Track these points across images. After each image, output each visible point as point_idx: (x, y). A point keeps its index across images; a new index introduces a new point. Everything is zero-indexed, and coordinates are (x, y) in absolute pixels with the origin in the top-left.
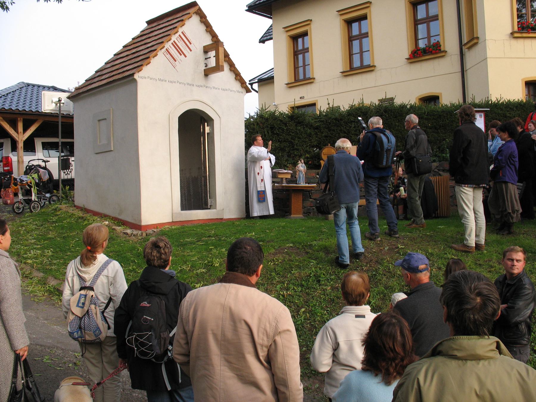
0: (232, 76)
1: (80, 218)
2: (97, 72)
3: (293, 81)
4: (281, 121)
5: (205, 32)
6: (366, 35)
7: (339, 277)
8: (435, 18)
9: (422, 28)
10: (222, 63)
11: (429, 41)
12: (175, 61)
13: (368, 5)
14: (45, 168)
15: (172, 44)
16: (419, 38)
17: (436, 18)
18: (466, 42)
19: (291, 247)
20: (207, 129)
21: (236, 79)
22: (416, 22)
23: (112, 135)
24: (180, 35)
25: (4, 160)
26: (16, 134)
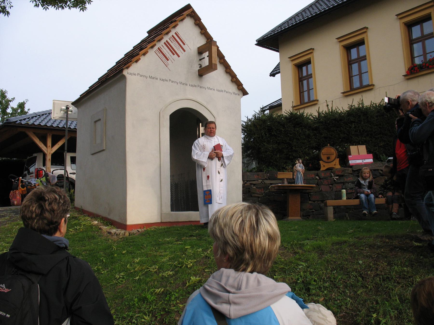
3: (299, 104)
4: (279, 123)
5: (200, 34)
6: (364, 58)
7: (335, 285)
11: (425, 58)
12: (168, 60)
15: (165, 43)
16: (415, 56)
21: (232, 81)
22: (411, 42)
24: (173, 36)
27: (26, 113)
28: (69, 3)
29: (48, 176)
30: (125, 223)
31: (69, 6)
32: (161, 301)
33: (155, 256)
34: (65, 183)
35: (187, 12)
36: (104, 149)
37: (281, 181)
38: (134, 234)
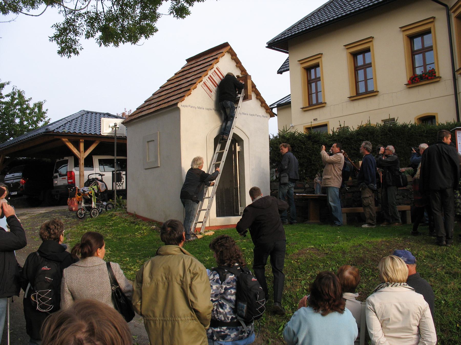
1: (132, 223)
2: (146, 102)
3: (307, 105)
4: (300, 141)
6: (370, 65)
8: (430, 49)
9: (418, 58)
10: (250, 93)
11: (425, 68)
12: (211, 92)
14: (101, 181)
15: (209, 78)
16: (416, 66)
17: (430, 49)
18: (458, 69)
19: (312, 248)
20: (238, 149)
22: (413, 53)
23: (159, 154)
24: (215, 71)
25: (68, 174)
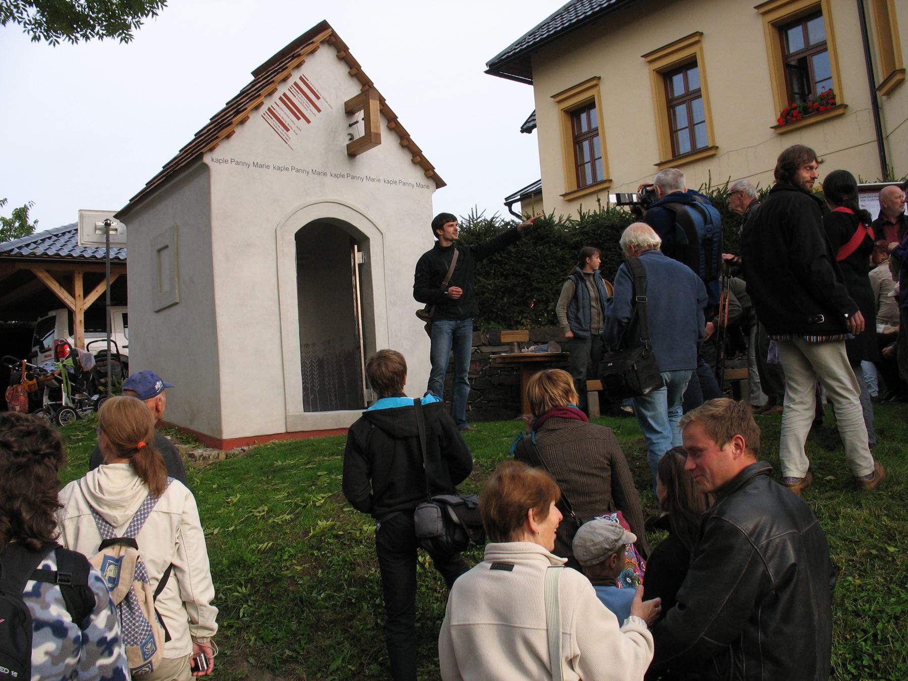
0: (403, 159)
3: (575, 188)
6: (697, 94)
12: (288, 130)
13: (696, 39)
15: (281, 99)
17: (822, 48)
18: (881, 80)
20: (358, 257)
21: (414, 162)
24: (296, 84)
26: (71, 299)
27: (31, 228)
28: (98, 28)
29: (77, 355)
30: (215, 435)
31: (98, 33)
32: (266, 562)
33: (266, 491)
34: (109, 367)
35: (321, 36)
36: (178, 301)
37: (507, 348)
38: (234, 455)
